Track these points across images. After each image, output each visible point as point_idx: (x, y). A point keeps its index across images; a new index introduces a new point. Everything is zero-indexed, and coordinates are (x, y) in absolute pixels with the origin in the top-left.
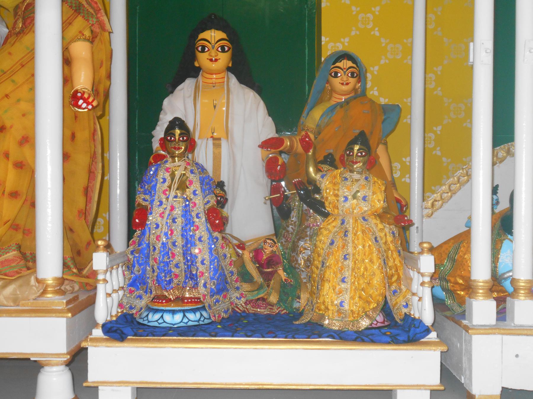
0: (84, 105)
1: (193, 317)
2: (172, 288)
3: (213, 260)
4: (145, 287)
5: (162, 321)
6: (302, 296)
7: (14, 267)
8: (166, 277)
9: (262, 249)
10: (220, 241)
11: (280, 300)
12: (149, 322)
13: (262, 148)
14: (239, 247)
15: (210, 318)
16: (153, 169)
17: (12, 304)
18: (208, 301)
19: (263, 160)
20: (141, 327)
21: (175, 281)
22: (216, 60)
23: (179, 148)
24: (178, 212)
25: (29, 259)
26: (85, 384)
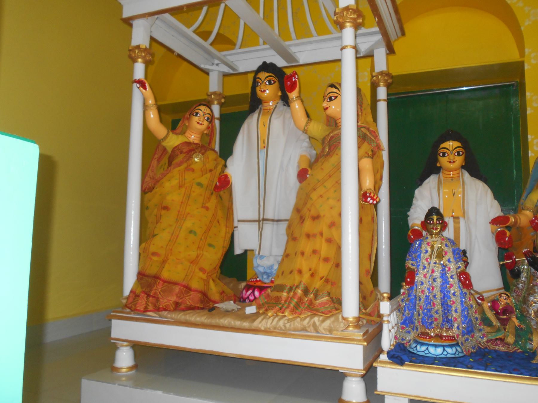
0: (371, 201)
1: (451, 351)
2: (433, 328)
3: (464, 310)
4: (413, 326)
5: (427, 352)
6: (534, 339)
7: (328, 308)
8: (428, 319)
9: (498, 300)
10: (468, 295)
11: (516, 342)
12: (418, 352)
13: (493, 224)
14: (479, 298)
15: (462, 352)
16: (418, 243)
17: (328, 333)
18: (461, 340)
19: (493, 233)
20: (414, 355)
21: (435, 323)
22: (454, 162)
23: (436, 229)
24: (437, 274)
25: (337, 303)
26: (375, 392)
